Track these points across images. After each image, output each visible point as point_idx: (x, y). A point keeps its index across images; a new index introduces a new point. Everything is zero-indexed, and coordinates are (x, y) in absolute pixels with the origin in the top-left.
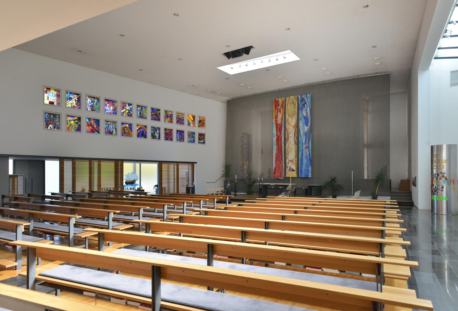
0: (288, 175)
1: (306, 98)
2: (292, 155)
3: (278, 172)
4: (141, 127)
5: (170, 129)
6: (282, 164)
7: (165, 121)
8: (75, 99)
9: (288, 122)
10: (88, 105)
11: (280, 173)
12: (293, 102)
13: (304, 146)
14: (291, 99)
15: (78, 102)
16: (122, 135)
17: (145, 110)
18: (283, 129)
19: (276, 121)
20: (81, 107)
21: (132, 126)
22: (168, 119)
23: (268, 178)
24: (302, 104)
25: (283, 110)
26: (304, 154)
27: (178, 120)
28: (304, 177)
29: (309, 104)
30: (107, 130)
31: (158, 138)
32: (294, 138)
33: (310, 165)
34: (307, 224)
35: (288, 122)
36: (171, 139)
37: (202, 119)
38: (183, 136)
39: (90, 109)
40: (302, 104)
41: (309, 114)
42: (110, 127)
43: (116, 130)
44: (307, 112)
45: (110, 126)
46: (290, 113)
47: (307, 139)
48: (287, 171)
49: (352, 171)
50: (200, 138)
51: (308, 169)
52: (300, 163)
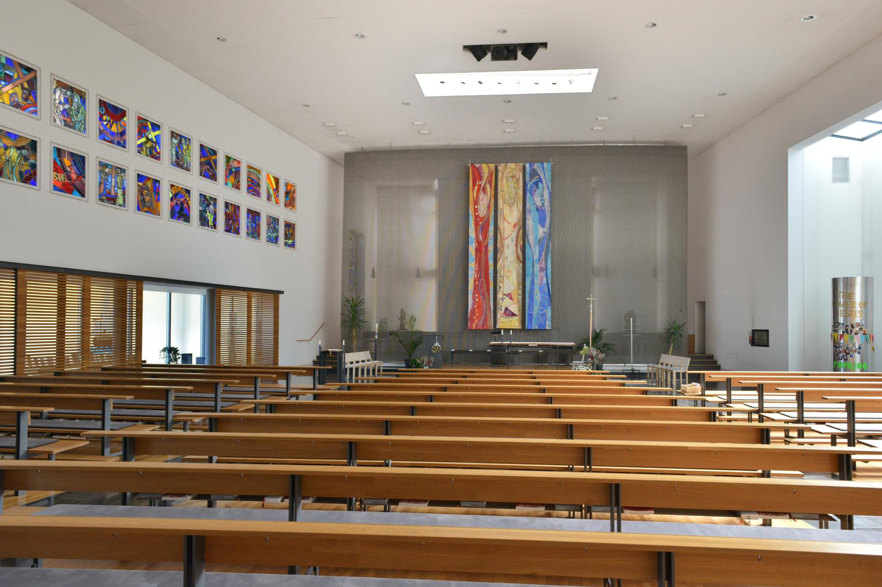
0: (501, 325)
1: (541, 172)
2: (509, 283)
3: (478, 318)
4: (179, 190)
5: (235, 205)
6: (489, 301)
7: (226, 184)
8: (21, 81)
9: (502, 216)
10: (57, 108)
11: (482, 319)
12: (514, 176)
13: (537, 267)
14: (510, 168)
15: (30, 95)
16: (139, 209)
17: (188, 149)
18: (491, 228)
19: (476, 210)
20: (38, 112)
21: (159, 185)
22: (232, 178)
23: (398, 330)
24: (533, 181)
25: (491, 188)
26: (537, 281)
27: (250, 183)
28: (536, 328)
29: (547, 183)
30: (102, 191)
31: (212, 224)
32: (515, 248)
33: (549, 305)
34: (271, 418)
35: (502, 216)
36: (237, 232)
37: (291, 189)
38: (259, 225)
39: (61, 121)
40: (532, 183)
41: (547, 203)
42: (111, 183)
43: (124, 194)
44: (541, 198)
45: (110, 179)
46: (507, 197)
47: (544, 253)
48: (499, 316)
49: (631, 319)
50: (287, 233)
51: (544, 311)
52: (527, 301)
